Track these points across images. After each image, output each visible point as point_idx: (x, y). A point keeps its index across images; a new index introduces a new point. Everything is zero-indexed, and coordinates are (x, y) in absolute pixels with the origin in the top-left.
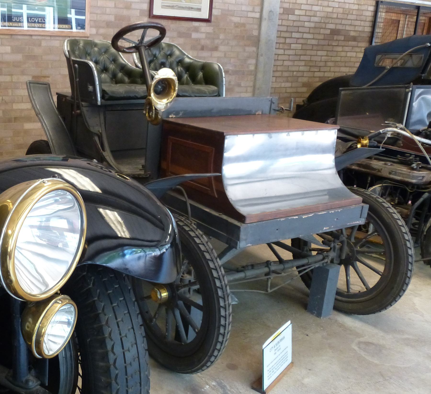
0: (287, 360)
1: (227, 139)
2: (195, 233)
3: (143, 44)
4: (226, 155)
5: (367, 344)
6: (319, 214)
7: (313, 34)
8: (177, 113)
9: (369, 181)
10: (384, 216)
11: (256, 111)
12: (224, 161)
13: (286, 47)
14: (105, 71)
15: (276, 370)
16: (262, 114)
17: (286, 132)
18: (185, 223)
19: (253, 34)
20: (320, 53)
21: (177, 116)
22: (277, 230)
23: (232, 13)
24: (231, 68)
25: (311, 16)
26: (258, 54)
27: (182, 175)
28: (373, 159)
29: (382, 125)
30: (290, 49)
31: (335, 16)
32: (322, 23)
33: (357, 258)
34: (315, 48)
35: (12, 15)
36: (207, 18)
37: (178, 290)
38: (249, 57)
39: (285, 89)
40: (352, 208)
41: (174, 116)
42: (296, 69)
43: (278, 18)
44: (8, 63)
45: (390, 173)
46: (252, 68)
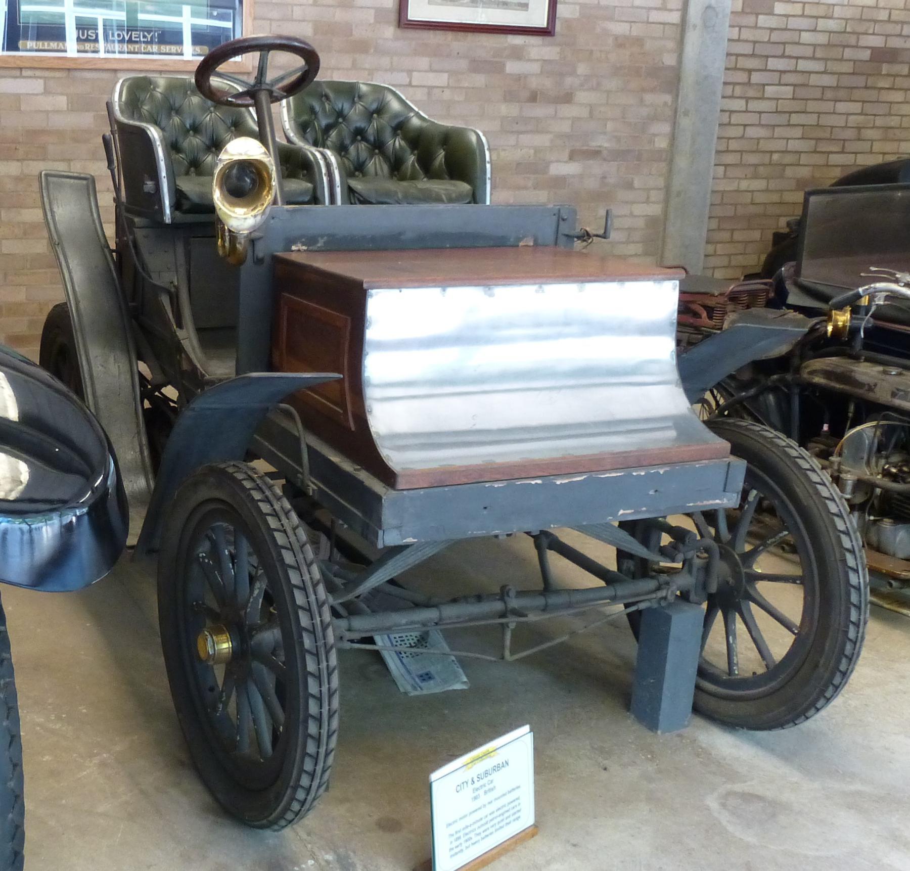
0: (519, 817)
1: (371, 296)
2: (272, 506)
3: (264, 87)
4: (371, 334)
5: (748, 797)
6: (602, 476)
7: (826, 60)
8: (310, 241)
9: (850, 415)
10: (799, 491)
11: (519, 239)
12: (367, 348)
13: (751, 93)
14: (214, 149)
15: (479, 838)
16: (536, 244)
17: (535, 284)
18: (258, 485)
19: (663, 63)
20: (841, 107)
21: (311, 248)
22: (485, 508)
23: (609, 14)
24: (606, 145)
25: (817, 17)
26: (676, 112)
27: (242, 376)
28: (862, 361)
29: (862, 274)
30: (762, 98)
31: (883, 15)
32: (849, 33)
33: (747, 592)
34: (829, 94)
35: (137, 27)
36: (545, 25)
37: (252, 637)
38: (654, 118)
39: (750, 194)
40: (697, 466)
41: (305, 248)
42: (780, 145)
43: (727, 24)
44: (60, 134)
45: (894, 395)
46: (662, 143)
